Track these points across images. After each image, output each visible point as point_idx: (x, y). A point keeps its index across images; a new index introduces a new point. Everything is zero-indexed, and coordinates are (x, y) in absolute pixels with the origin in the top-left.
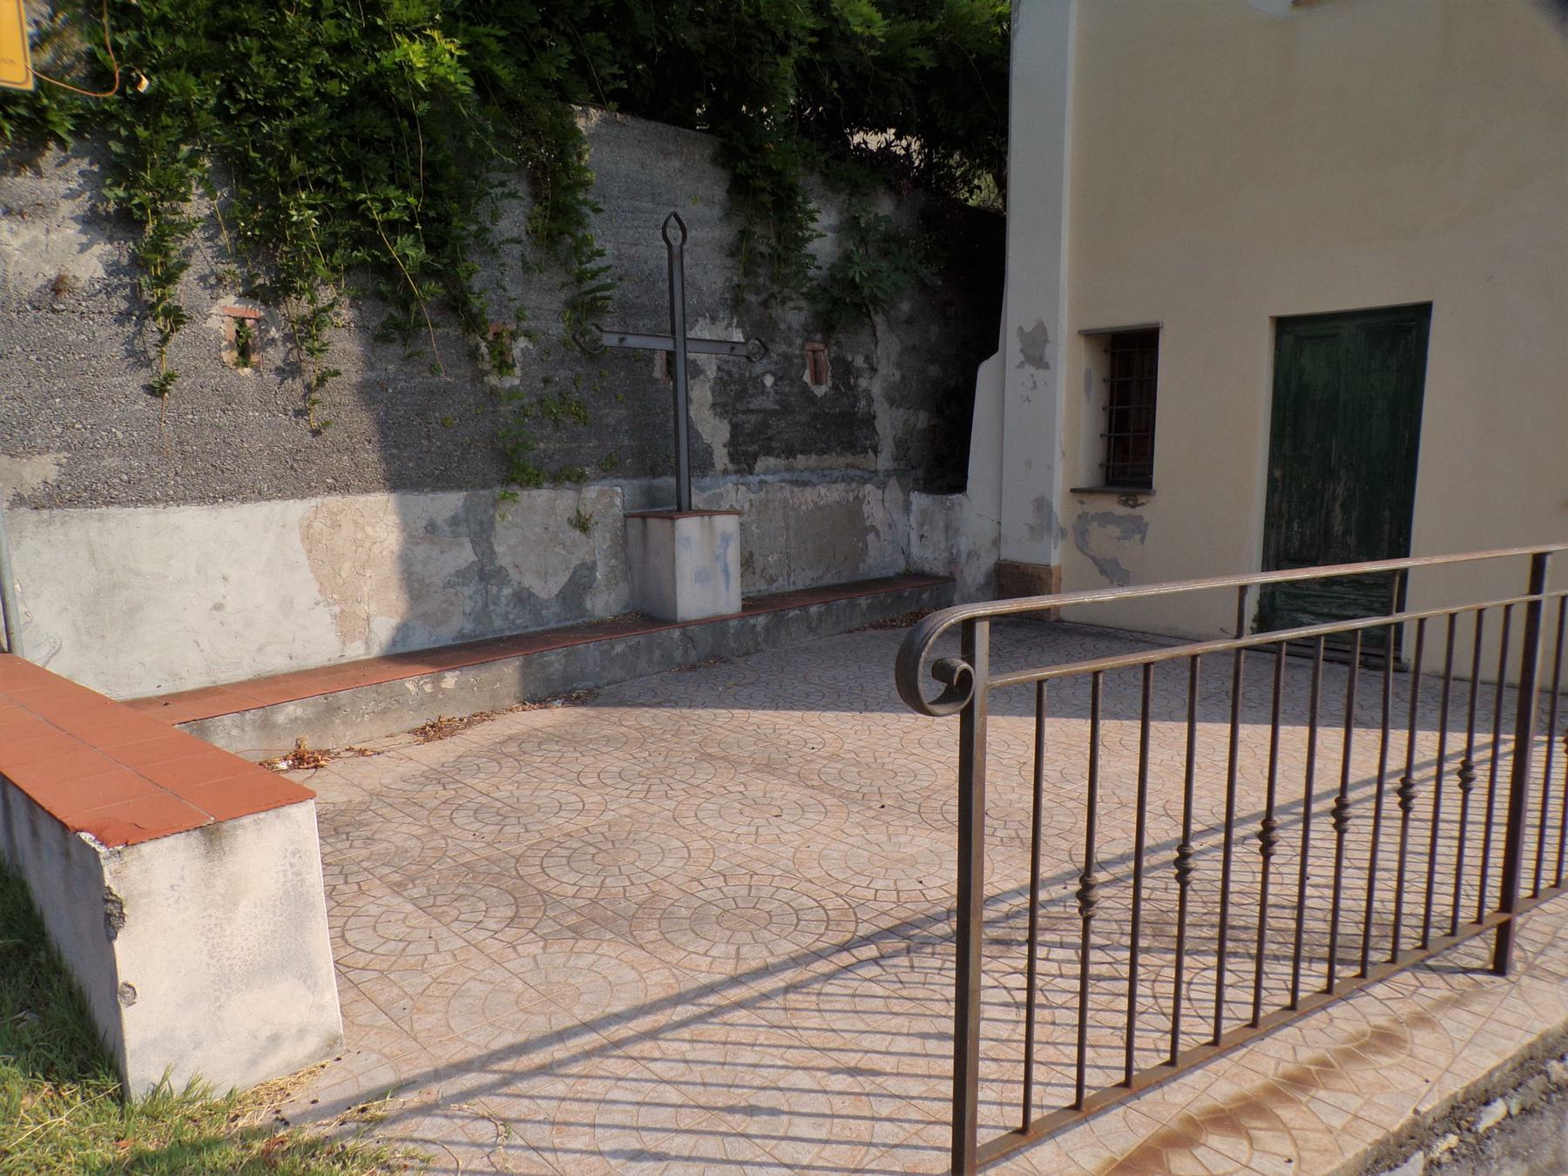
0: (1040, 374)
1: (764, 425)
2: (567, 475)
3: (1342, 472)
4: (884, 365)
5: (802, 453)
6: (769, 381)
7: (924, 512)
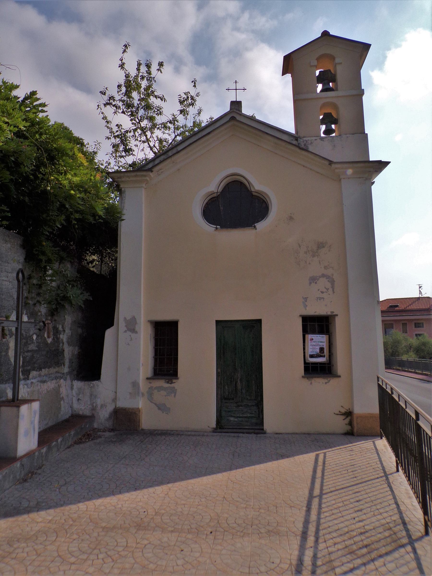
0: (133, 335)
1: (33, 356)
3: (239, 370)
6: (35, 337)
7: (79, 389)
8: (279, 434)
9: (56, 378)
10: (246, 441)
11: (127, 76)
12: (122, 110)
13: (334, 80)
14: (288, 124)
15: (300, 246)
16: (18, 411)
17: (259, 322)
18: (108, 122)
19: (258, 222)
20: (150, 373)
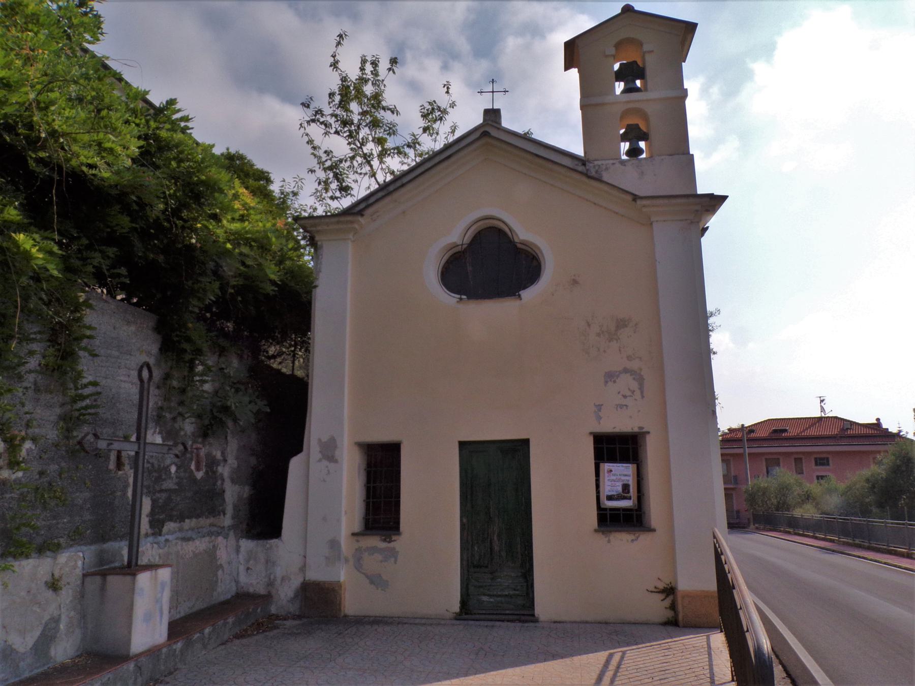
0: (332, 466)
2: (48, 547)
4: (229, 457)
5: (188, 518)
6: (173, 469)
8: (560, 622)
9: (210, 534)
10: (506, 633)
11: (344, 79)
12: (334, 130)
13: (642, 76)
14: (573, 142)
15: (589, 325)
16: (134, 582)
17: (526, 442)
18: (314, 148)
19: (525, 288)
20: (357, 526)
